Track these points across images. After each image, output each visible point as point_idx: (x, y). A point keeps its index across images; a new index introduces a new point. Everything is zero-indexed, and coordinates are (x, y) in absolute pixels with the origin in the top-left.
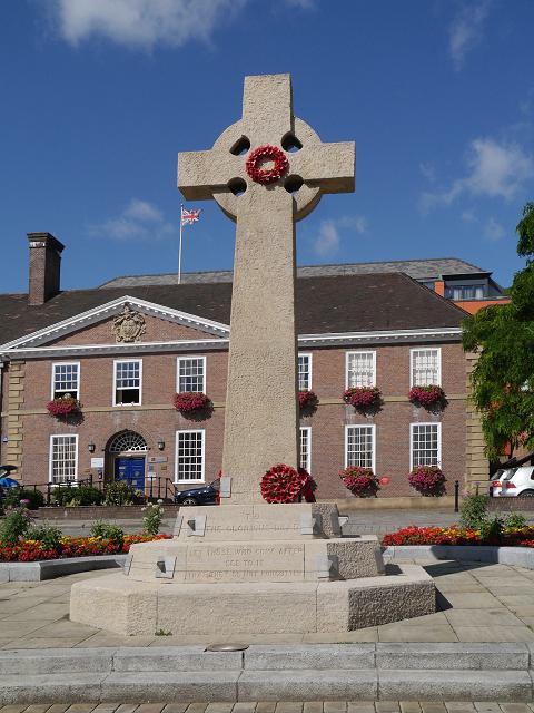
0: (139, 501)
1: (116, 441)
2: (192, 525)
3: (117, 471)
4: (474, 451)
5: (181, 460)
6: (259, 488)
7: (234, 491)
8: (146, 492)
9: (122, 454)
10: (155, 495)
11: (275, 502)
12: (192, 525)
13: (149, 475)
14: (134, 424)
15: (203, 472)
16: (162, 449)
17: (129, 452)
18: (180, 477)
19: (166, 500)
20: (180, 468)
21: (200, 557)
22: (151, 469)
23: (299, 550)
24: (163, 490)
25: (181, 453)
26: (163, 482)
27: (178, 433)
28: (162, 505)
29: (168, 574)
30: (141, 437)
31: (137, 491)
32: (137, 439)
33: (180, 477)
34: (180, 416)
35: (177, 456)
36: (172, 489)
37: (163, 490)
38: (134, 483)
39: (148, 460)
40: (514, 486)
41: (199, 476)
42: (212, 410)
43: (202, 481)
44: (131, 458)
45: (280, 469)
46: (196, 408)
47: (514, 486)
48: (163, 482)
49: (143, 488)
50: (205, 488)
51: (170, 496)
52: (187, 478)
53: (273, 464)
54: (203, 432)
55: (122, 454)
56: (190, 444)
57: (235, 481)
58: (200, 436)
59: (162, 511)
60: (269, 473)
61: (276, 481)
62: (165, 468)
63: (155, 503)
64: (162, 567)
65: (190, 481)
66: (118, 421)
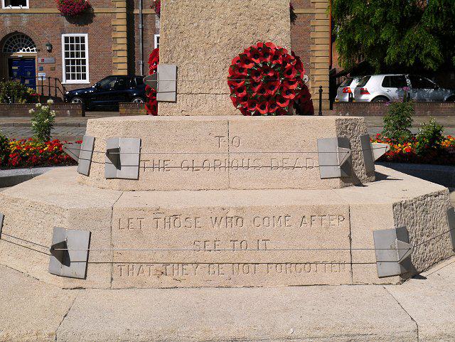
0: (31, 100)
1: (8, 43)
2: (114, 156)
3: (11, 71)
4: (317, 60)
5: (67, 62)
6: (226, 88)
7: (182, 90)
8: (38, 91)
9: (14, 55)
10: (46, 94)
11: (258, 114)
12: (114, 156)
13: (40, 76)
14: (23, 25)
15: (87, 73)
16: (50, 51)
17: (21, 53)
18: (68, 78)
19: (56, 99)
20: (67, 69)
21: (139, 232)
22: (41, 69)
23: (340, 217)
24: (53, 89)
25: (67, 55)
26: (53, 83)
27: (63, 36)
28: (52, 107)
29: (76, 268)
30: (31, 40)
31: (29, 89)
32: (27, 41)
33: (68, 78)
34: (64, 20)
35: (64, 58)
36: (61, 88)
37: (53, 89)
38: (27, 82)
39: (38, 61)
40: (367, 92)
41: (84, 78)
42: (93, 15)
43: (87, 81)
44: (23, 59)
45: (262, 51)
46: (79, 13)
47: (367, 92)
48: (53, 83)
49: (34, 87)
50: (91, 88)
51: (60, 95)
52: (73, 78)
53: (248, 42)
54: (86, 36)
55: (14, 55)
56: (74, 46)
57: (180, 69)
58: (83, 39)
59: (53, 113)
60: (244, 59)
61: (257, 74)
62: (53, 69)
63: (44, 103)
64: (61, 253)
65: (76, 81)
66: (8, 23)
